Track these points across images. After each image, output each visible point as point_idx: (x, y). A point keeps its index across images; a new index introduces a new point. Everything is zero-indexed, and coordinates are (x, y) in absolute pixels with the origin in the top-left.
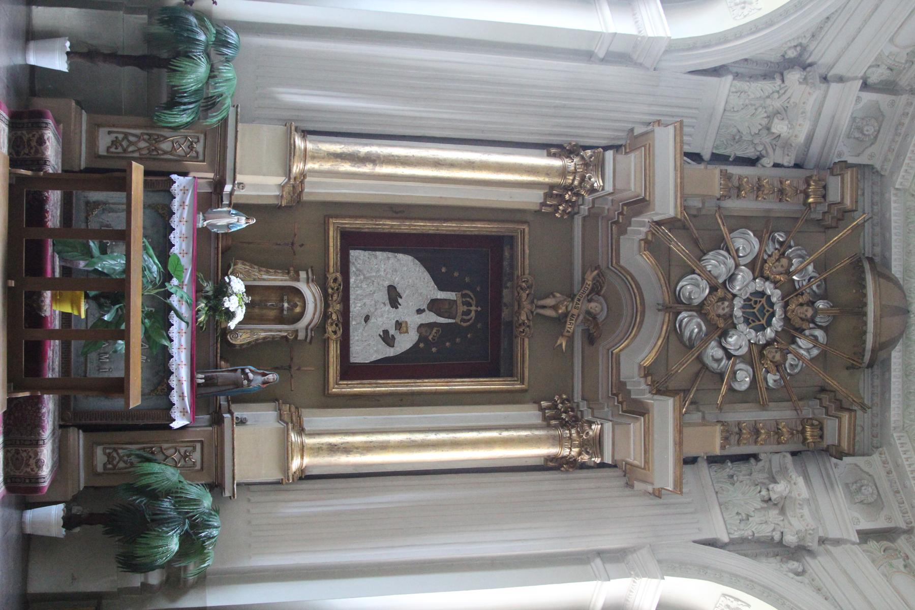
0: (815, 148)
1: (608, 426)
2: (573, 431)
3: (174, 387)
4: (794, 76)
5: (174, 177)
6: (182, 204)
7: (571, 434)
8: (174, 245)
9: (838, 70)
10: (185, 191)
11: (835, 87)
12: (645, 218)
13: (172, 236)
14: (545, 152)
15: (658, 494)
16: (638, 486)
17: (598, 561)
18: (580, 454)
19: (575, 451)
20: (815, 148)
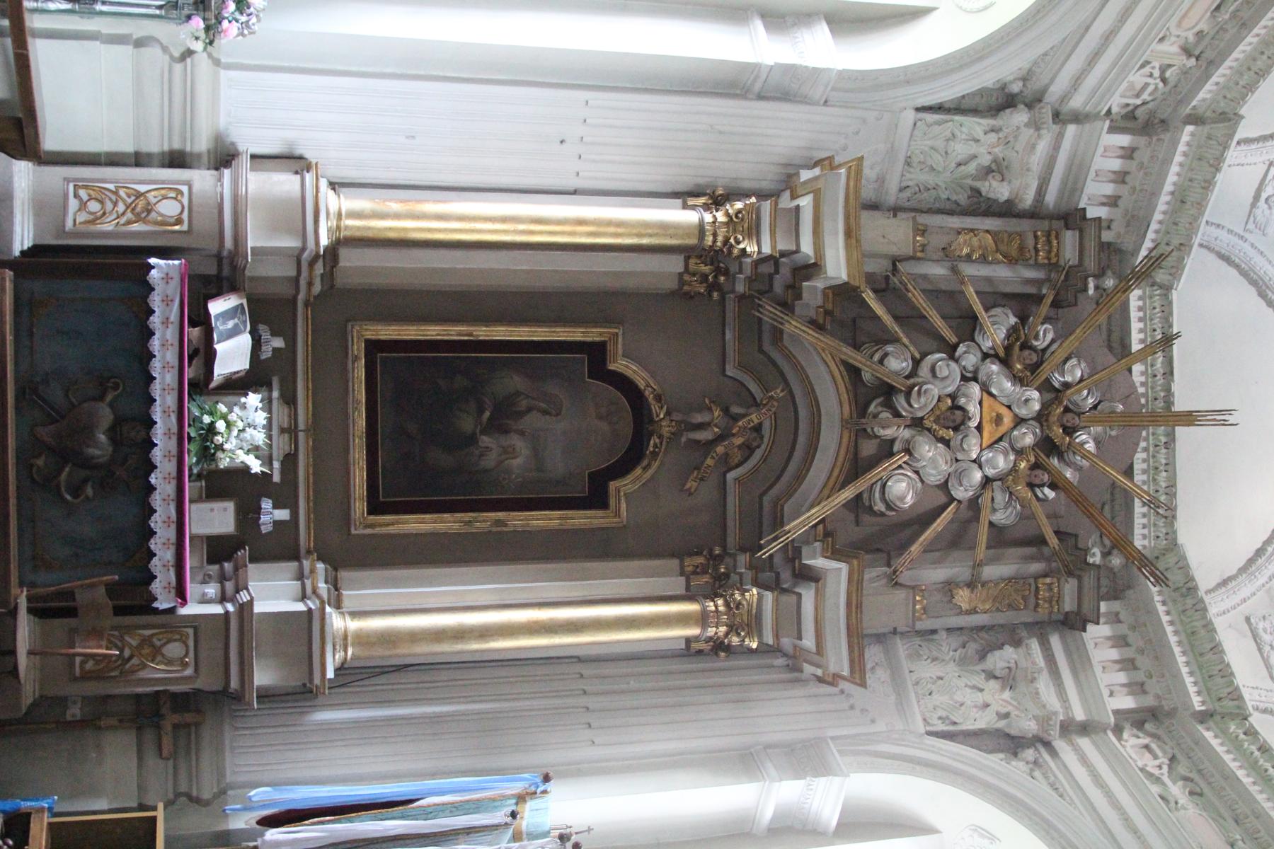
0: (1051, 198)
1: (769, 596)
2: (720, 602)
3: (157, 398)
4: (1019, 117)
5: (153, 261)
6: (166, 322)
7: (716, 606)
8: (155, 577)
9: (1076, 102)
10: (167, 278)
11: (1071, 129)
12: (819, 284)
13: (152, 541)
14: (679, 202)
15: (831, 680)
16: (809, 669)
17: (758, 25)
18: (727, 634)
19: (723, 629)
20: (1051, 198)
